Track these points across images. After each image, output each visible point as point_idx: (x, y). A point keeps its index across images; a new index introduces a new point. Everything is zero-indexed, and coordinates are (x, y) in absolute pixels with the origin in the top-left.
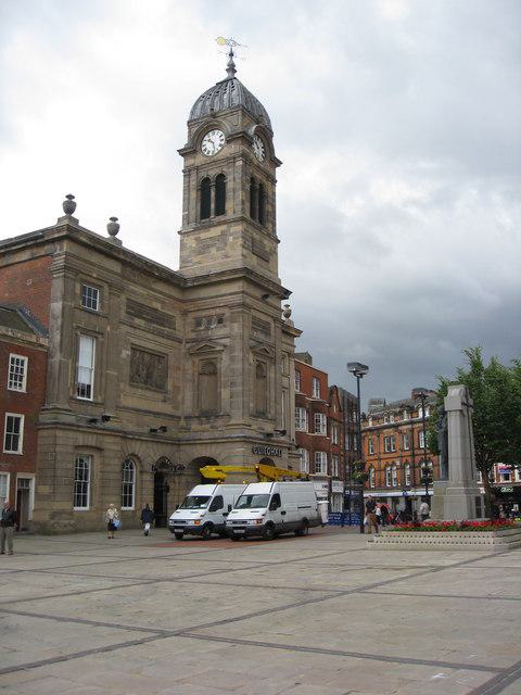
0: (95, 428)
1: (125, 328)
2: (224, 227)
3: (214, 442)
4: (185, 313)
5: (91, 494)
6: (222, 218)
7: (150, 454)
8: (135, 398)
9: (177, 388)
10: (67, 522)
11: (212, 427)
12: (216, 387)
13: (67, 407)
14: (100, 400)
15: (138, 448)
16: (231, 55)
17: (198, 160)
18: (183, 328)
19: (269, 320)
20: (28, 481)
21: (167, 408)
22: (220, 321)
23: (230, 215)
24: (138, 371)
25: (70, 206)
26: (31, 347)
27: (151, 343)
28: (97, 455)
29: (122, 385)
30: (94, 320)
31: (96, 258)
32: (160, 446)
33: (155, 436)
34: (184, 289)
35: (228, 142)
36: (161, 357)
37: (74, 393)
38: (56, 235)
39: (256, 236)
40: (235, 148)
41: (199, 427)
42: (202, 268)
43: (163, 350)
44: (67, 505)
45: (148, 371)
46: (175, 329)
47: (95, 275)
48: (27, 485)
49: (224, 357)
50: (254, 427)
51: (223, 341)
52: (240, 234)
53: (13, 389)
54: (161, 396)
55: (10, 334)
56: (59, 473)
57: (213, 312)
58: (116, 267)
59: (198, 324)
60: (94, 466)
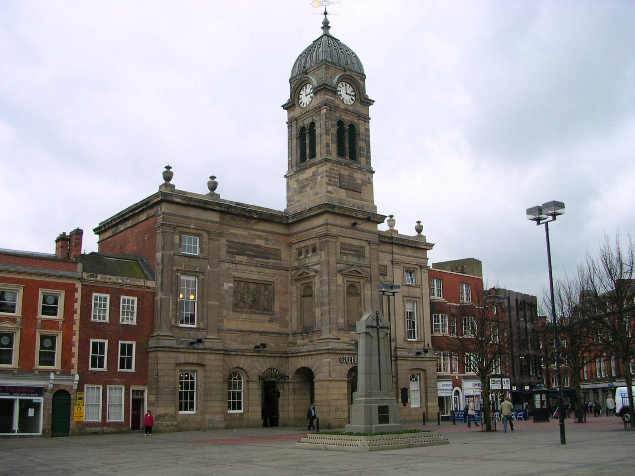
0: (194, 349)
1: (226, 265)
2: (314, 169)
3: (309, 354)
4: (290, 245)
5: (244, 400)
6: (312, 161)
7: (258, 366)
8: (235, 321)
9: (285, 310)
10: (169, 423)
11: (310, 341)
12: (313, 307)
13: (170, 334)
14: (202, 325)
15: (242, 362)
16: (326, 13)
17: (297, 112)
18: (288, 257)
19: (364, 244)
20: (142, 392)
21: (275, 327)
23: (318, 157)
24: (242, 299)
25: (168, 176)
26: (138, 289)
27: (254, 274)
28: (200, 369)
29: (225, 312)
30: (194, 262)
31: (192, 213)
32: (266, 359)
33: (259, 352)
34: (288, 225)
35: (315, 94)
36: (267, 285)
37: (176, 322)
38: (156, 200)
39: (343, 172)
40: (320, 99)
42: (300, 206)
43: (269, 279)
44: (171, 410)
45: (253, 298)
46: (280, 260)
47: (192, 227)
48: (143, 395)
50: (343, 339)
52: (325, 174)
53: (125, 322)
54: (267, 318)
55: (120, 281)
56: (161, 385)
58: (215, 217)
59: (300, 254)
60: (198, 378)
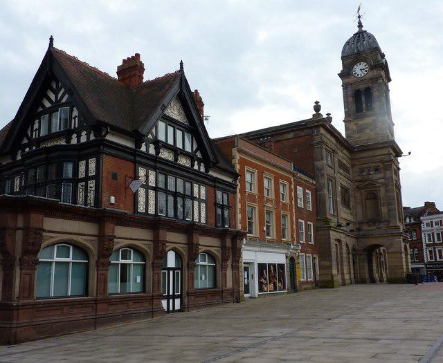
3: (381, 236)
16: (359, 17)
22: (376, 170)
25: (317, 108)
41: (368, 228)
49: (381, 189)
51: (379, 181)
57: (372, 165)
